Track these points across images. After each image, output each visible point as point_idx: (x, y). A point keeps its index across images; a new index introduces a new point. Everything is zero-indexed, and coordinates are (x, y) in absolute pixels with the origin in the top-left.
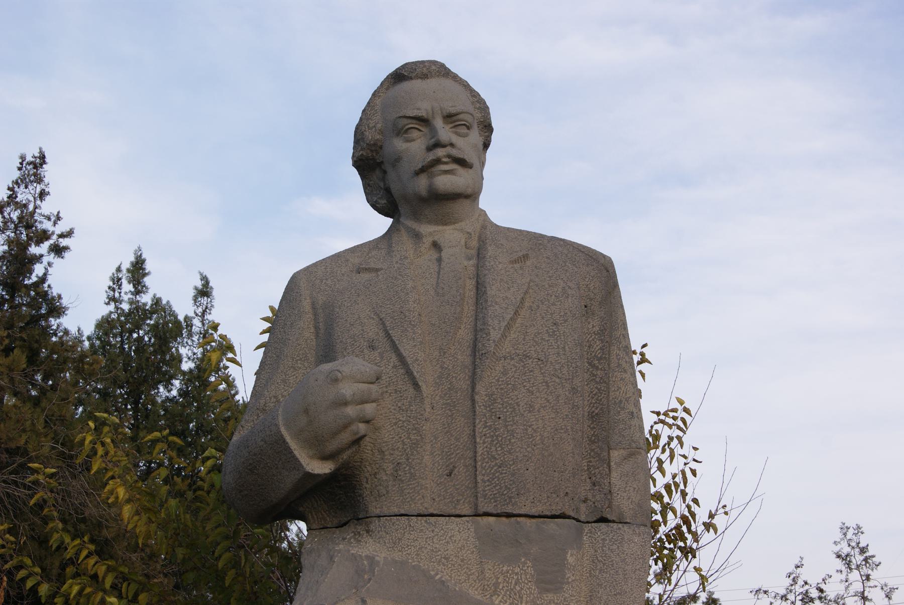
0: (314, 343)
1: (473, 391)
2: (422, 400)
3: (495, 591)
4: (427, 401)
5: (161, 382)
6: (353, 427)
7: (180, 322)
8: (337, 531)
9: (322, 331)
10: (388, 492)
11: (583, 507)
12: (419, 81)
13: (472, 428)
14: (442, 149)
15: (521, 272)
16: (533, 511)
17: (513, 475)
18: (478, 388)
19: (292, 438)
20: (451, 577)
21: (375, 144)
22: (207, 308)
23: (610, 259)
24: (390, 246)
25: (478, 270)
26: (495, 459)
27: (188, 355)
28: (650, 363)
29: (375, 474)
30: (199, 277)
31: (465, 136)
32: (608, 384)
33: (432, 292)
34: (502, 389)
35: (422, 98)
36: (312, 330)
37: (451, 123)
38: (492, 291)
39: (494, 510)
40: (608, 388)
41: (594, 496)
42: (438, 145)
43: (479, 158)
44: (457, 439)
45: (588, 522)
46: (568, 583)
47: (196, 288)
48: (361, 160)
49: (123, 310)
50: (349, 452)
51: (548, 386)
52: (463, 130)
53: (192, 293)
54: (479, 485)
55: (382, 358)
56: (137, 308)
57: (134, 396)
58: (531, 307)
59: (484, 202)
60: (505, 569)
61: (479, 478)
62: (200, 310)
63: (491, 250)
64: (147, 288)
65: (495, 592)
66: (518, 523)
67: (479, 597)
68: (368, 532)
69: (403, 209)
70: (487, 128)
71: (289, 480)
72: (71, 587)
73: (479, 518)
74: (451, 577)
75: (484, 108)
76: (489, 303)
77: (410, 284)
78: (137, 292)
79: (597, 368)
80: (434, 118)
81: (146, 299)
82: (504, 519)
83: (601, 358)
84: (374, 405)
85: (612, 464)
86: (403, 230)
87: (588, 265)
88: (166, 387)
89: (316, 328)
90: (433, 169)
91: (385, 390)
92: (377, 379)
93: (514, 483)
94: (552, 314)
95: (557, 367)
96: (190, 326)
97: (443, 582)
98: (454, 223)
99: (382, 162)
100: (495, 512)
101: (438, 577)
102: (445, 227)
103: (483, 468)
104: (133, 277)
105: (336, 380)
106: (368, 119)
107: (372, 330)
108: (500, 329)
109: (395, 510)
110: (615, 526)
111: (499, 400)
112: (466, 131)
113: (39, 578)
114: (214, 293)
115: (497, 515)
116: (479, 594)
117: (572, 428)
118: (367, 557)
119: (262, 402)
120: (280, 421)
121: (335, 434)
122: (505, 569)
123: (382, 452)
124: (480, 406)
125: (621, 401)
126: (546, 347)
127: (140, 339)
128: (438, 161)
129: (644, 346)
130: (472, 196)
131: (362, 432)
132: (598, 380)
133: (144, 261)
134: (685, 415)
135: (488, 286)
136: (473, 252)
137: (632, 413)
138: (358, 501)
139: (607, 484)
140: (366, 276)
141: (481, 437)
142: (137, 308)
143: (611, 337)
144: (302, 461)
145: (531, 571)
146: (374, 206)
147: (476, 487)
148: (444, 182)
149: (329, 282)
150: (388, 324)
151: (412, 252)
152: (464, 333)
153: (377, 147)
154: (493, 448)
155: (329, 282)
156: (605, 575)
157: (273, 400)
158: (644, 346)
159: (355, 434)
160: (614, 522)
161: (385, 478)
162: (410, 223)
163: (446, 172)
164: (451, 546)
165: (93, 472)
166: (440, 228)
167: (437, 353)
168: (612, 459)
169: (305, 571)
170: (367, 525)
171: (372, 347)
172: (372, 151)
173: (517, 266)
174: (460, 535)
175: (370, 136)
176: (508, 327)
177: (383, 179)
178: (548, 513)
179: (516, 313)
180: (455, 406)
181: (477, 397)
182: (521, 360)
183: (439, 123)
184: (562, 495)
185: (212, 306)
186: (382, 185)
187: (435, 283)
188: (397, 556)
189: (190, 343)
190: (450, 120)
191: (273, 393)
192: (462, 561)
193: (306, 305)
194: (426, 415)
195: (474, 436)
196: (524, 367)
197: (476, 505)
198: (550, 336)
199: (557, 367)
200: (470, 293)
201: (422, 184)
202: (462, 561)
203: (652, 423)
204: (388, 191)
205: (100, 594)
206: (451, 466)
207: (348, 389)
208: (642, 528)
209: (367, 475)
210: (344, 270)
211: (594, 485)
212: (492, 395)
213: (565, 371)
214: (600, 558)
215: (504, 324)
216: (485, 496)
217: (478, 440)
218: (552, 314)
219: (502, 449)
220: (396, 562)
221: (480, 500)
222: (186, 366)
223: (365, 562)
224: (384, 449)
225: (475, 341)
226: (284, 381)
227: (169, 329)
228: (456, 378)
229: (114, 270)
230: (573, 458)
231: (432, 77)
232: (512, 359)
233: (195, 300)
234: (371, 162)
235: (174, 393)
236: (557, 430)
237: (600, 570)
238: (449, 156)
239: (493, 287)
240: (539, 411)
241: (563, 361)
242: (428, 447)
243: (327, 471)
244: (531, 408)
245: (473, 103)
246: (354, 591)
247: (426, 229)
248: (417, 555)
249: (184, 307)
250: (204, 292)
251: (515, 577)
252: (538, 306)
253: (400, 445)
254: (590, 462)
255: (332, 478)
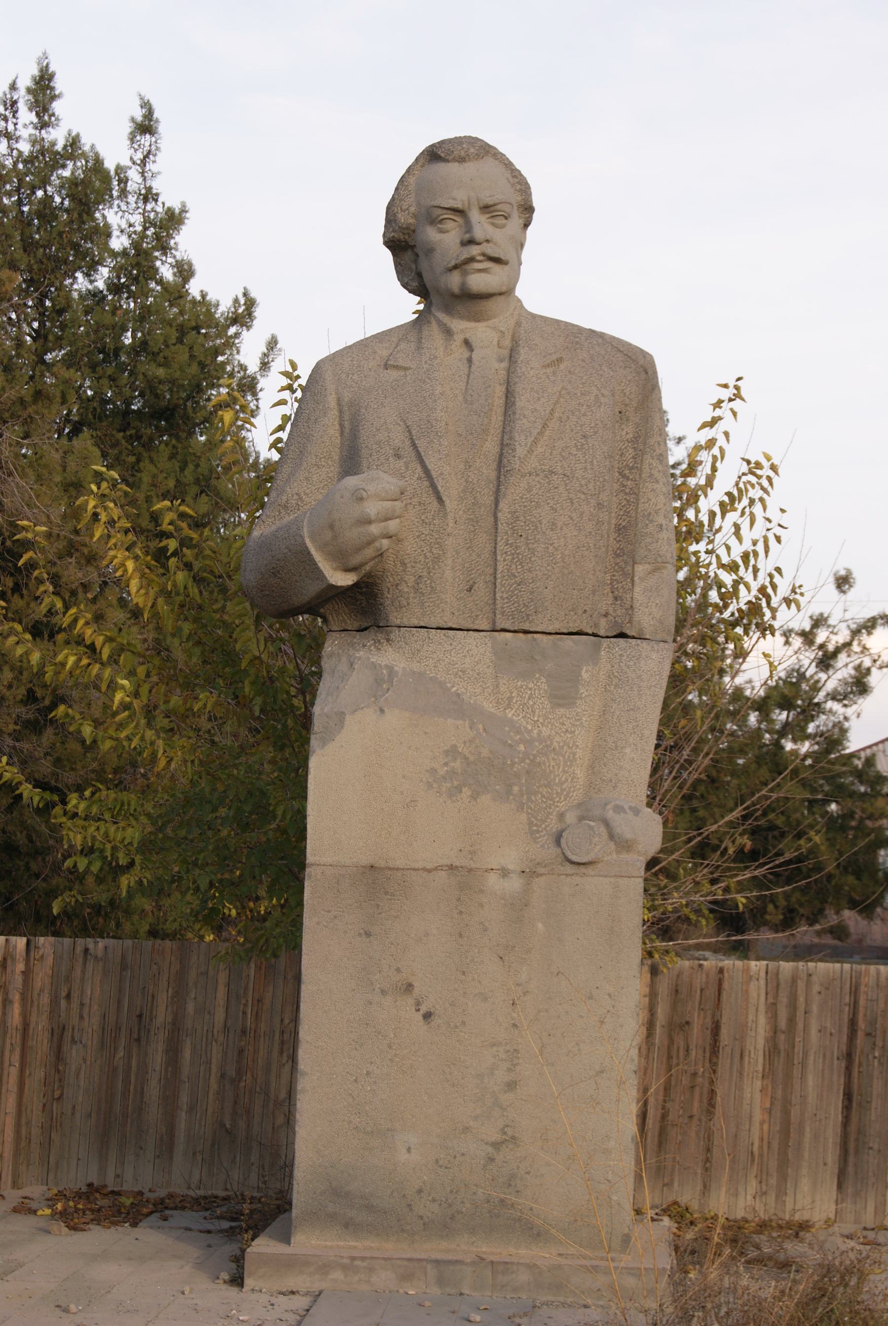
0: (338, 441)
1: (496, 507)
2: (445, 515)
3: (509, 704)
4: (450, 516)
5: (80, 268)
6: (377, 544)
7: (108, 172)
8: (358, 634)
9: (347, 430)
10: (408, 604)
11: (603, 622)
12: (456, 164)
13: (493, 544)
14: (477, 247)
15: (552, 378)
16: (550, 629)
17: (532, 593)
18: (501, 505)
19: (316, 550)
20: (466, 689)
21: (407, 228)
22: (149, 152)
23: (651, 356)
24: (420, 340)
25: (508, 376)
26: (515, 576)
27: (120, 222)
28: (743, 400)
29: (397, 585)
30: (138, 102)
31: (502, 227)
32: (637, 495)
33: (460, 398)
34: (525, 506)
35: (459, 184)
36: (337, 427)
37: (488, 213)
38: (521, 402)
39: (511, 626)
40: (638, 500)
41: (615, 611)
42: (471, 242)
43: (517, 253)
44: (479, 556)
45: (607, 637)
46: (581, 698)
47: (133, 120)
48: (393, 241)
49: (20, 153)
50: (371, 563)
51: (572, 503)
52: (500, 221)
53: (128, 128)
54: (498, 602)
55: (407, 468)
56: (42, 151)
57: (35, 283)
58: (560, 418)
59: (521, 291)
60: (519, 684)
61: (498, 595)
62: (139, 156)
63: (523, 353)
64: (57, 119)
65: (509, 706)
66: (535, 640)
67: (492, 710)
68: (388, 640)
69: (434, 297)
70: (528, 210)
71: (311, 590)
72: (66, 657)
73: (496, 633)
74: (466, 689)
75: (523, 187)
76: (517, 416)
77: (439, 390)
78: (43, 125)
79: (628, 479)
80: (469, 208)
81: (57, 136)
82: (521, 635)
83: (632, 468)
84: (398, 520)
85: (636, 578)
86: (434, 324)
87: (625, 367)
88: (87, 275)
89: (342, 426)
90: (467, 267)
91: (409, 501)
92: (402, 493)
93: (532, 600)
94: (581, 426)
95: (583, 482)
96: (123, 181)
97: (458, 695)
98: (487, 320)
99: (415, 246)
100: (512, 629)
101: (454, 689)
102: (477, 324)
103: (503, 586)
104: (36, 101)
105: (361, 499)
106: (401, 200)
107: (398, 438)
108: (526, 444)
109: (415, 622)
110: (633, 641)
111: (522, 518)
112: (504, 221)
113: (30, 645)
114: (162, 128)
115: (515, 632)
116: (493, 707)
117: (595, 545)
118: (387, 666)
119: (284, 498)
120: (306, 532)
121: (359, 549)
122: (519, 684)
123: (404, 564)
124: (502, 524)
125: (650, 514)
126: (573, 462)
127: (48, 198)
128: (472, 260)
129: (739, 379)
130: (507, 292)
131: (385, 547)
132: (627, 491)
133: (51, 77)
134: (771, 474)
135: (517, 396)
136: (506, 352)
137: (661, 525)
138: (380, 609)
139: (629, 599)
140: (394, 374)
141: (502, 555)
142: (42, 151)
143: (645, 444)
144: (326, 573)
145: (545, 686)
146: (405, 286)
147: (494, 603)
148: (478, 282)
149: (355, 377)
150: (414, 432)
151: (442, 349)
152: (491, 446)
153: (410, 231)
154: (514, 566)
155: (355, 377)
156: (619, 691)
157: (295, 497)
158: (739, 379)
159: (378, 551)
160: (634, 637)
161: (406, 590)
162: (441, 316)
163: (480, 271)
164: (468, 660)
165: (95, 539)
166: (473, 324)
167: (462, 466)
168: (636, 574)
169: (326, 676)
170: (388, 634)
171: (398, 456)
172: (404, 234)
173: (549, 370)
174: (477, 649)
175: (403, 218)
176: (535, 442)
177: (416, 261)
178: (565, 631)
179: (545, 426)
180: (477, 522)
181: (499, 515)
182: (546, 476)
183: (476, 216)
184: (580, 612)
185: (158, 149)
186: (414, 267)
187: (464, 388)
188: (416, 667)
189: (124, 208)
190: (487, 210)
191: (295, 490)
192: (478, 674)
193: (332, 401)
194: (449, 530)
195: (495, 553)
196: (549, 483)
197: (494, 622)
198: (578, 450)
199: (583, 482)
200: (499, 401)
201: (454, 281)
202: (478, 674)
203: (736, 479)
204: (419, 275)
205: (98, 666)
206: (471, 582)
207: (372, 508)
208: (662, 644)
209: (389, 585)
210: (371, 364)
211: (616, 599)
212: (515, 512)
213: (591, 486)
214: (616, 674)
215: (530, 440)
216: (503, 613)
217: (499, 558)
218: (581, 426)
219: (523, 567)
220: (414, 673)
221: (498, 616)
222: (118, 242)
223: (385, 671)
224: (406, 561)
225: (501, 455)
226: (307, 479)
227: (95, 185)
228: (480, 492)
229: (6, 88)
230: (594, 575)
231: (470, 160)
232: (538, 475)
233: (132, 140)
234: (403, 244)
235: (101, 285)
236: (578, 548)
237: (616, 686)
238: (484, 255)
239: (522, 398)
240: (561, 529)
241: (590, 476)
242: (449, 562)
243: (350, 583)
244: (553, 526)
245: (513, 185)
246: (373, 699)
247: (459, 325)
248: (435, 667)
249: (115, 152)
250: (146, 126)
251: (529, 692)
252: (568, 418)
253: (422, 558)
254: (614, 576)
255: (356, 585)
